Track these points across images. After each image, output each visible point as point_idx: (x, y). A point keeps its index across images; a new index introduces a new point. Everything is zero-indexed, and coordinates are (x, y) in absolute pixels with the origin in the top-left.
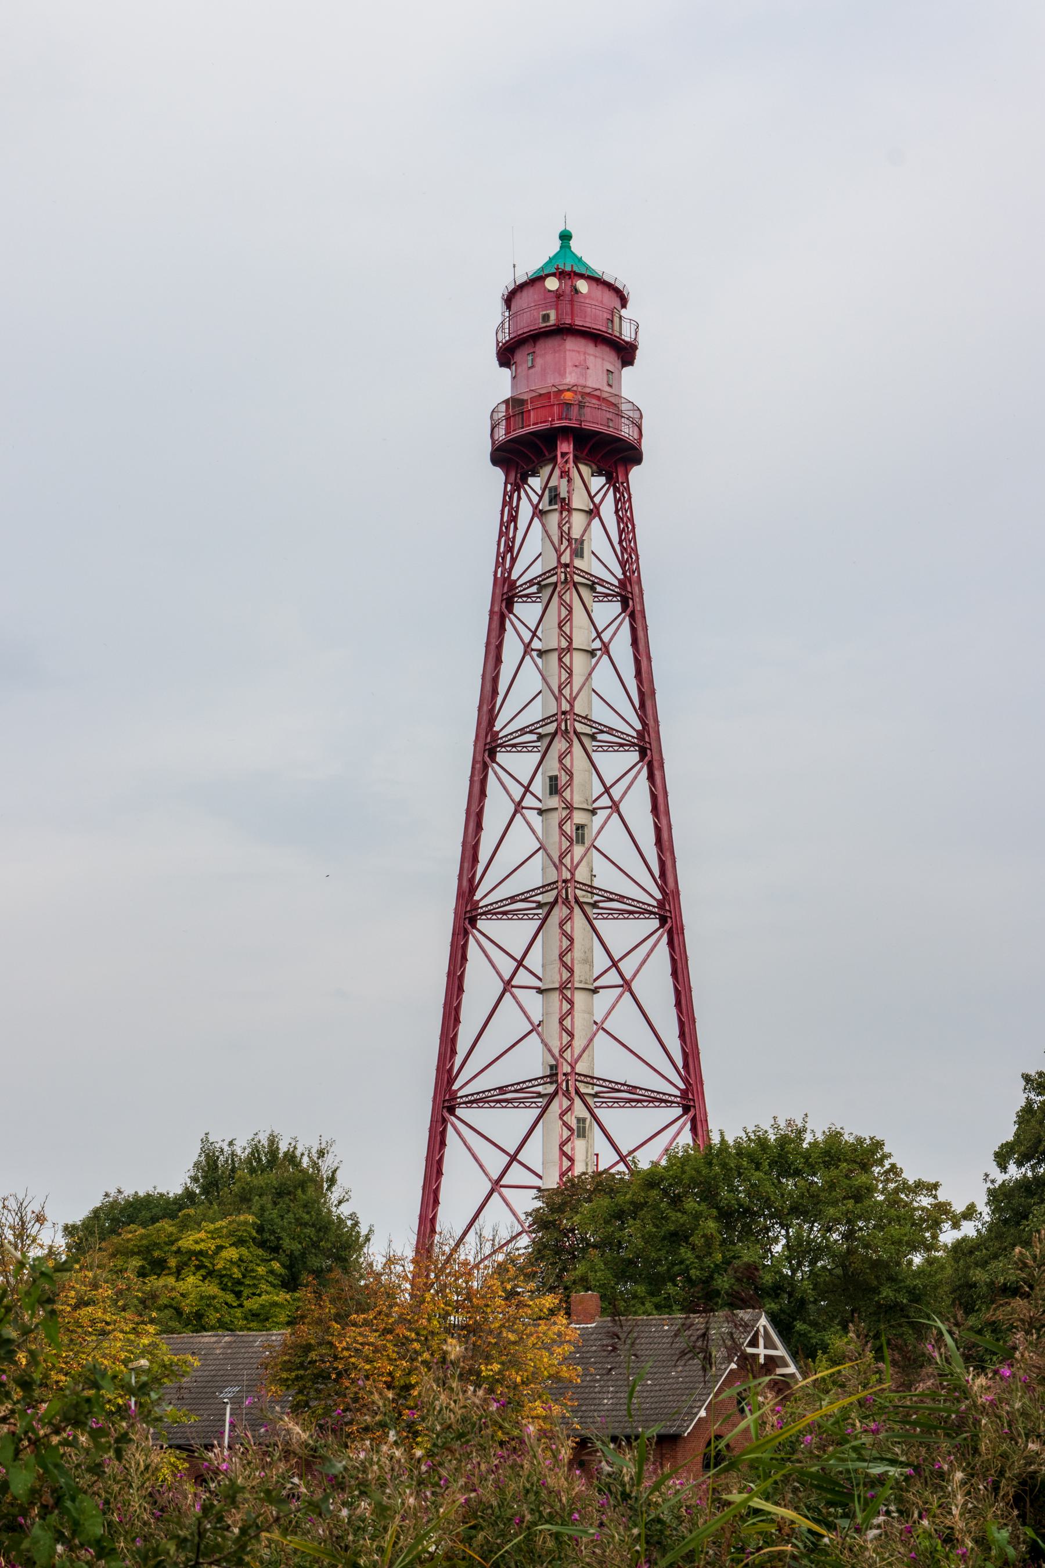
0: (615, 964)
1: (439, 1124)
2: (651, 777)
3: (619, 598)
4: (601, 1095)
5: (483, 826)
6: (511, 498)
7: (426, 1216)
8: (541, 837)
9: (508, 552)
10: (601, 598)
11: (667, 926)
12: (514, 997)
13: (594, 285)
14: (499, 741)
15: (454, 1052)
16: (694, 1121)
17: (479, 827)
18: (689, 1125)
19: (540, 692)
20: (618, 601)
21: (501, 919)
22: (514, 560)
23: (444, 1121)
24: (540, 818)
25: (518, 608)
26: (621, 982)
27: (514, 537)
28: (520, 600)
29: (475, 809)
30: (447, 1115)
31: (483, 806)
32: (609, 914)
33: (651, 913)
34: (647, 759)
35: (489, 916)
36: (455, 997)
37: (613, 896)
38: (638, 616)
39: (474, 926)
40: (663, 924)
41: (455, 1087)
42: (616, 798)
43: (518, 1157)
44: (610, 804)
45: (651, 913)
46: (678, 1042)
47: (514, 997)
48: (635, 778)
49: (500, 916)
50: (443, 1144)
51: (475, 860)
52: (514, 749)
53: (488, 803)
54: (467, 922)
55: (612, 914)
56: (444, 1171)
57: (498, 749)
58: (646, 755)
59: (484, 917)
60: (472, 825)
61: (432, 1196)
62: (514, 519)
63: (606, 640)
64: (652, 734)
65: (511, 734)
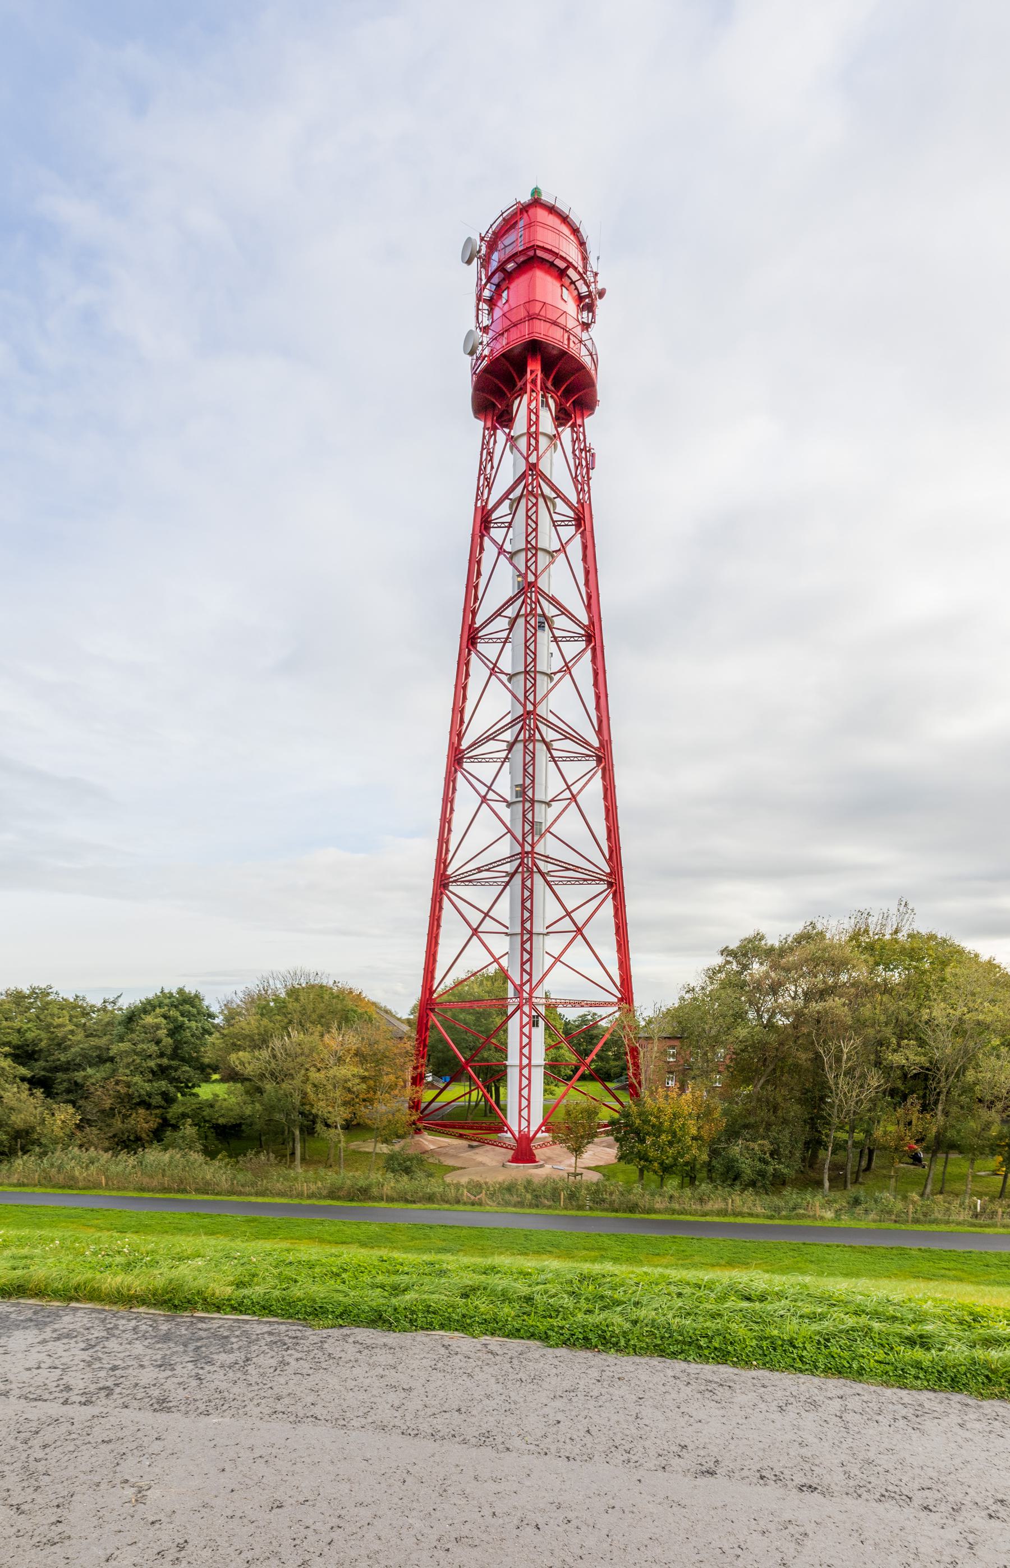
0: (568, 914)
2: (594, 660)
3: (573, 523)
4: (552, 874)
6: (488, 443)
8: (509, 826)
11: (602, 765)
12: (489, 805)
17: (465, 698)
19: (509, 712)
24: (509, 810)
26: (575, 929)
28: (496, 525)
33: (601, 880)
34: (602, 765)
37: (571, 867)
38: (588, 534)
42: (575, 793)
44: (570, 796)
45: (601, 880)
46: (606, 842)
47: (489, 805)
51: (462, 722)
57: (479, 640)
62: (490, 454)
63: (575, 791)
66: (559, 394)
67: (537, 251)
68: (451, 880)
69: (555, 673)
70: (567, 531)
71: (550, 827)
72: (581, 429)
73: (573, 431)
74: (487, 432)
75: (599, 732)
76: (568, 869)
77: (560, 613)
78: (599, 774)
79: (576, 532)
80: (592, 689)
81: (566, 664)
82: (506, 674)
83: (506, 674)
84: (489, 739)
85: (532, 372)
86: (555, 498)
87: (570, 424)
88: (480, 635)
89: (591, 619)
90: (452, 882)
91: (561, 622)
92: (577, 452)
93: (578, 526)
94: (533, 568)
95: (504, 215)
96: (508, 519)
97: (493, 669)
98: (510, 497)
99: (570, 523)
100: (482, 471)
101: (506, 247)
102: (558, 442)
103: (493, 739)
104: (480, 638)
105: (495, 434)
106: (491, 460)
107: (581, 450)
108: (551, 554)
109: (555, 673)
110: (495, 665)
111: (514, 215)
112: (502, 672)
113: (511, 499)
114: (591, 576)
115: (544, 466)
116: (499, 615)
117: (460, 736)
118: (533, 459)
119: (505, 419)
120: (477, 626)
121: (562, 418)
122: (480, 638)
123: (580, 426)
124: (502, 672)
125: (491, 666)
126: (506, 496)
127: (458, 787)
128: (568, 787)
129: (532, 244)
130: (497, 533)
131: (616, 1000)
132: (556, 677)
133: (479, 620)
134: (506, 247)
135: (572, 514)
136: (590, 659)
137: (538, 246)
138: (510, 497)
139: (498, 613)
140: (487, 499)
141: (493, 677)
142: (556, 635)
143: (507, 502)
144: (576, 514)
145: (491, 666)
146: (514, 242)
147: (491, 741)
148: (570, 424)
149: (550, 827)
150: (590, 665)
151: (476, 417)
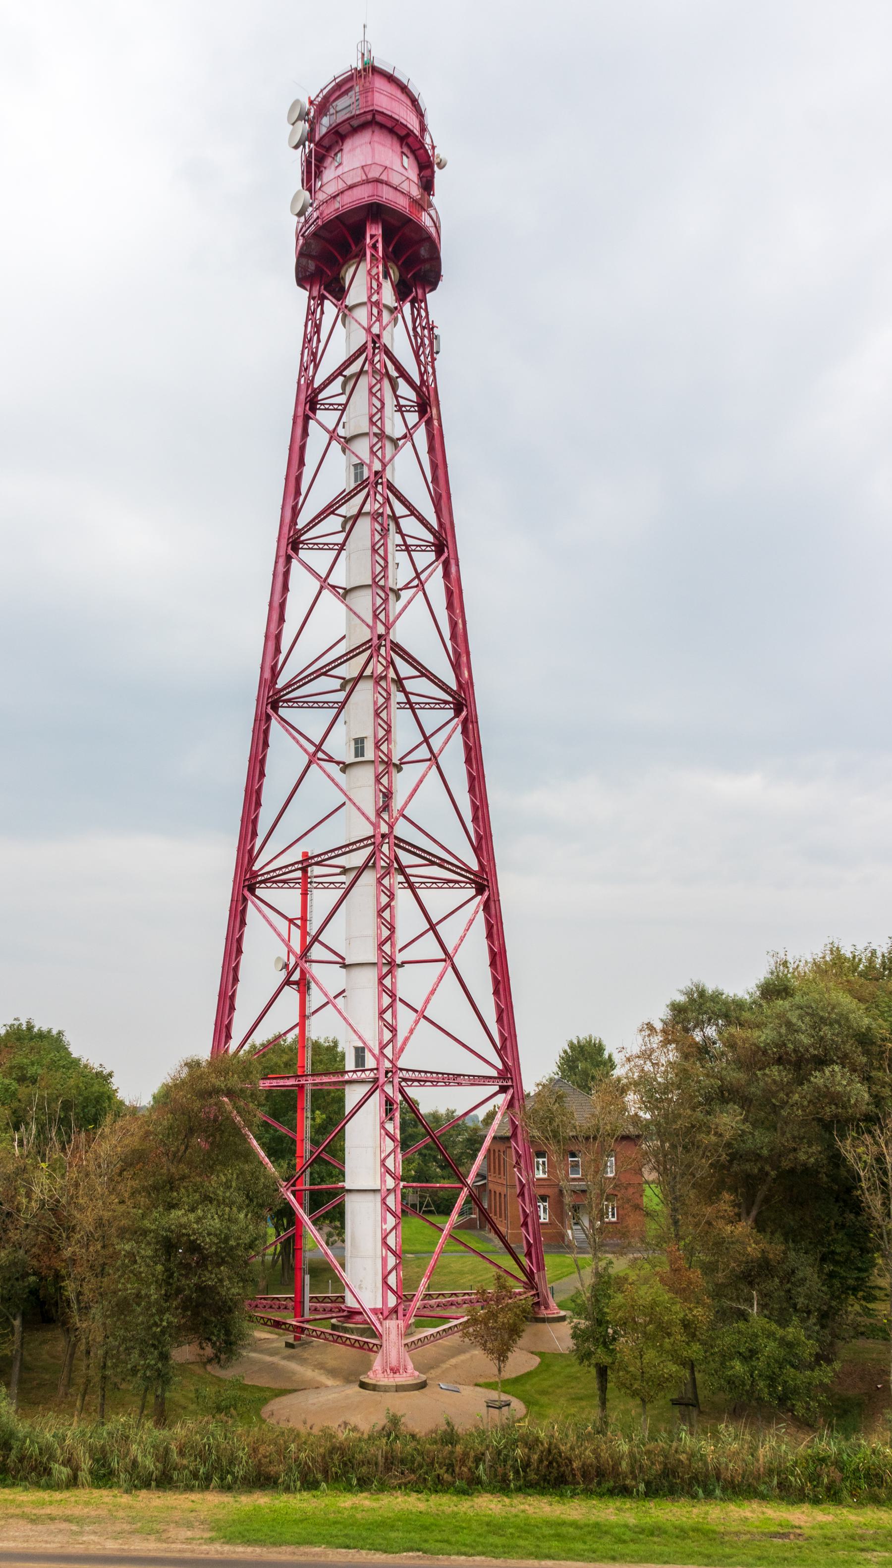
1: (263, 722)
2: (446, 575)
3: (433, 548)
5: (286, 617)
7: (226, 993)
9: (315, 333)
10: (440, 885)
11: (426, 418)
13: (682, 1407)
14: (260, 878)
15: (255, 834)
16: (465, 723)
17: (282, 619)
18: (459, 729)
20: (451, 708)
21: (282, 888)
22: (316, 367)
23: (245, 900)
25: (320, 414)
26: (443, 956)
27: (317, 348)
29: (274, 631)
30: (247, 894)
31: (281, 630)
32: (433, 883)
34: (443, 558)
35: (269, 885)
36: (223, 1044)
39: (253, 893)
40: (458, 713)
41: (255, 868)
43: (319, 938)
44: (428, 755)
46: (445, 613)
48: (431, 574)
49: (280, 885)
50: (243, 923)
51: (278, 651)
52: (286, 885)
53: (309, 440)
54: (246, 889)
55: (435, 883)
56: (240, 978)
57: (301, 546)
58: (443, 552)
59: (263, 885)
60: (275, 617)
61: (262, 736)
62: (317, 328)
64: (449, 533)
65: (280, 869)
66: (400, 263)
67: (376, 116)
68: (260, 878)
69: (399, 439)
70: (413, 418)
71: (403, 808)
72: (423, 305)
73: (413, 307)
74: (312, 302)
75: (456, 666)
76: (432, 863)
77: (418, 674)
78: (440, 570)
79: (420, 419)
80: (488, 971)
81: (418, 575)
82: (338, 763)
83: (338, 763)
84: (323, 672)
85: (372, 237)
86: (397, 377)
87: (410, 298)
88: (302, 538)
89: (441, 524)
90: (285, 701)
91: (419, 686)
92: (419, 330)
93: (439, 552)
94: (379, 454)
95: (337, 81)
96: (340, 538)
97: (315, 753)
98: (344, 373)
99: (412, 409)
100: (307, 341)
101: (337, 112)
102: (400, 316)
103: (325, 674)
104: (302, 542)
105: (322, 304)
106: (318, 332)
107: (423, 328)
108: (395, 442)
109: (399, 439)
110: (319, 748)
111: (350, 79)
112: (331, 760)
113: (345, 376)
114: (440, 472)
115: (386, 340)
116: (333, 513)
117: (296, 512)
118: (375, 330)
119: (339, 292)
120: (299, 527)
121: (403, 291)
122: (302, 542)
123: (422, 301)
124: (331, 760)
125: (312, 749)
126: (339, 372)
127: (248, 919)
128: (426, 740)
129: (371, 108)
130: (327, 417)
131: (494, 1073)
132: (401, 443)
133: (302, 522)
134: (337, 112)
135: (430, 538)
136: (442, 575)
137: (377, 111)
138: (344, 373)
139: (330, 510)
140: (313, 376)
141: (314, 767)
142: (408, 543)
143: (340, 379)
144: (418, 394)
145: (312, 749)
146: (345, 107)
147: (323, 677)
148: (410, 298)
149: (403, 808)
150: (484, 944)
151: (104, 1078)
